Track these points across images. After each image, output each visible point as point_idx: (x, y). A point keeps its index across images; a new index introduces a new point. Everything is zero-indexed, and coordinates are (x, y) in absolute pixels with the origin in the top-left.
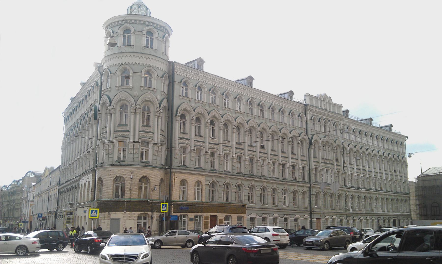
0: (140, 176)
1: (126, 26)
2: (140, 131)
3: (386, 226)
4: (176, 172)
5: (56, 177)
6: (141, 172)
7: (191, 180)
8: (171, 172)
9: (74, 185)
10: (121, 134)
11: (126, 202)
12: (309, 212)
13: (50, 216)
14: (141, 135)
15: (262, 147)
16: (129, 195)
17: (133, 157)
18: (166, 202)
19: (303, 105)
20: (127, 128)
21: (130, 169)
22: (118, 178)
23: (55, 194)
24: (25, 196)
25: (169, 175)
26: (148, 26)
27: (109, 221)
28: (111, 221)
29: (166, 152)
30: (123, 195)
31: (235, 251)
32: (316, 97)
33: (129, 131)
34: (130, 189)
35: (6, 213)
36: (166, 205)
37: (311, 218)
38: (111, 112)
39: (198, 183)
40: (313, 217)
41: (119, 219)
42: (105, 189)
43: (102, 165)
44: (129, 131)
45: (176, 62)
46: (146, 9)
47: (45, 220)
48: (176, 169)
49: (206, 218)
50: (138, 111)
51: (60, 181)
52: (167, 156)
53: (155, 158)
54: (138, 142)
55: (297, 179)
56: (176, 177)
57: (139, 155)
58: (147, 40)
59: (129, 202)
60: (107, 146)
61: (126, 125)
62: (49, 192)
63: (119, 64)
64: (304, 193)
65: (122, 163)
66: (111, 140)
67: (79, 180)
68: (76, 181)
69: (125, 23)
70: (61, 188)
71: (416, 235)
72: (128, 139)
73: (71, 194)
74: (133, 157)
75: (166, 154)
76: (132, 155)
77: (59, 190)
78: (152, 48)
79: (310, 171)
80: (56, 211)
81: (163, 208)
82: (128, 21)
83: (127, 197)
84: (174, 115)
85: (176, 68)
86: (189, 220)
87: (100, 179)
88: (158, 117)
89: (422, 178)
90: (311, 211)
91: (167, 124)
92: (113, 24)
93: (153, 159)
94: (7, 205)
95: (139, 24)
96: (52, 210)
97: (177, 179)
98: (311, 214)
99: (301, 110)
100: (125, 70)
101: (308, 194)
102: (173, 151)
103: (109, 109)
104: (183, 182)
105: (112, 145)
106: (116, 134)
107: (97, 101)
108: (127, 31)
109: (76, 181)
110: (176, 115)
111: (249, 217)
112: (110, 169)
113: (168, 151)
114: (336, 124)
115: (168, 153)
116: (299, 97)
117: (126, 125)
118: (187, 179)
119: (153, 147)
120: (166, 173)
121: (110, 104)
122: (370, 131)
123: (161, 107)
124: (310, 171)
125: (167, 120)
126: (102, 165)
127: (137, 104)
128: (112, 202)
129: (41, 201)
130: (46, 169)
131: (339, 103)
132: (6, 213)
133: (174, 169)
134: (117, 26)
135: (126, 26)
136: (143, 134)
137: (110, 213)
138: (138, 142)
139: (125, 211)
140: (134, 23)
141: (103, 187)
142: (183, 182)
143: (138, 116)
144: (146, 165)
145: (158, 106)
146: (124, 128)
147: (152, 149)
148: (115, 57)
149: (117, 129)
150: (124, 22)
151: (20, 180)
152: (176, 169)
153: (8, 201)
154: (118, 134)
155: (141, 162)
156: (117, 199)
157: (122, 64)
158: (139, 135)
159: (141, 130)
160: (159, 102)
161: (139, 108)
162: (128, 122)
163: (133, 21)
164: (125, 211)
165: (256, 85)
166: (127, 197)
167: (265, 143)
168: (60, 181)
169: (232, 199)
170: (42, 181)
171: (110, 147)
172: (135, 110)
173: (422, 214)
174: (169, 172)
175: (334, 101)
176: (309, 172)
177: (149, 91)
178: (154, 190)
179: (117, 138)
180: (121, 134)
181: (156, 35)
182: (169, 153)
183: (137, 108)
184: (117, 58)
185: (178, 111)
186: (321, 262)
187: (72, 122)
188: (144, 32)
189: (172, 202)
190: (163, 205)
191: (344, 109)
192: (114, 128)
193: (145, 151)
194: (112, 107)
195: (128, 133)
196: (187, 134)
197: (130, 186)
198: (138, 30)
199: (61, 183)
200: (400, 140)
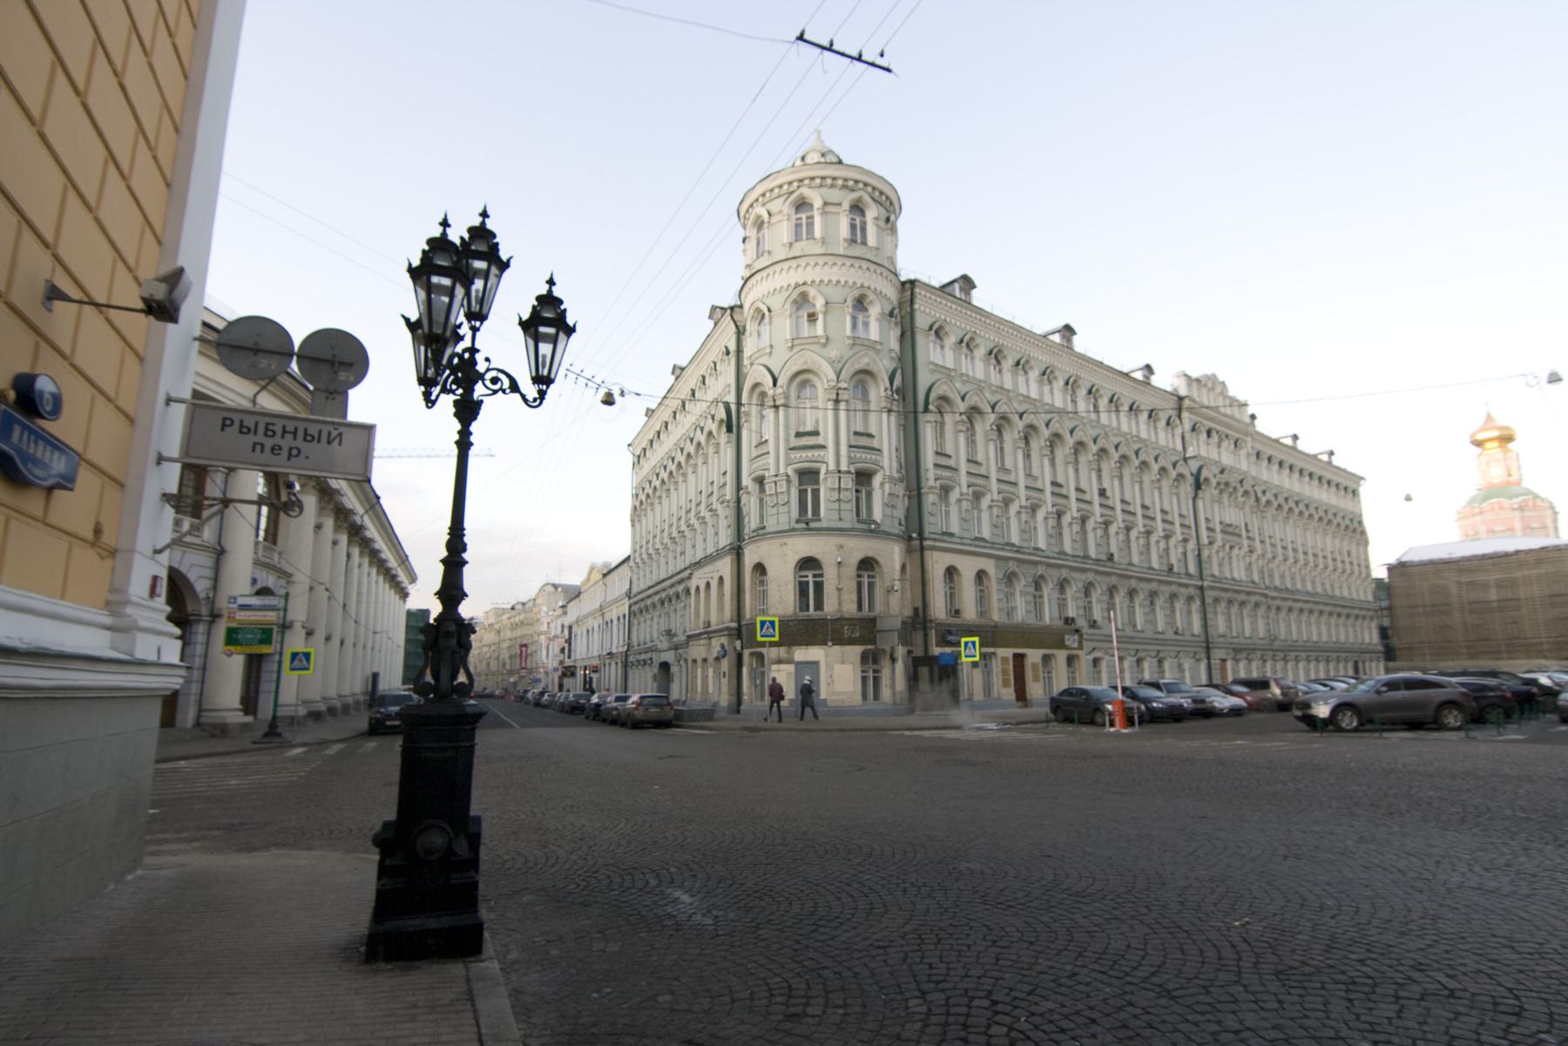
0: (858, 556)
1: (801, 194)
2: (851, 446)
3: (1342, 673)
4: (933, 548)
5: (619, 584)
6: (860, 548)
7: (967, 567)
8: (922, 549)
9: (642, 604)
11: (831, 620)
12: (1204, 644)
13: (610, 664)
14: (852, 455)
15: (1102, 493)
16: (836, 603)
17: (840, 510)
19: (1176, 398)
20: (820, 440)
21: (834, 541)
22: (808, 563)
23: (619, 618)
24: (545, 628)
25: (917, 555)
26: (853, 190)
29: (906, 499)
30: (819, 605)
31: (432, 696)
32: (1198, 380)
33: (823, 447)
34: (839, 589)
35: (508, 662)
36: (974, 643)
37: (1209, 658)
38: (779, 402)
39: (981, 576)
40: (1212, 656)
41: (816, 663)
42: (772, 589)
43: (761, 533)
44: (823, 447)
45: (919, 281)
47: (596, 671)
48: (935, 540)
49: (1005, 660)
50: (843, 396)
51: (630, 589)
52: (908, 510)
53: (888, 511)
54: (849, 472)
55: (1175, 570)
56: (934, 559)
58: (853, 227)
59: (840, 620)
60: (773, 485)
62: (603, 615)
63: (789, 286)
64: (1190, 599)
65: (812, 525)
66: (782, 471)
67: (689, 578)
68: (681, 581)
69: (799, 187)
70: (636, 603)
72: (825, 465)
73: (642, 620)
74: (840, 510)
75: (906, 504)
76: (836, 506)
77: (630, 607)
78: (864, 243)
80: (628, 650)
82: (807, 182)
83: (830, 606)
84: (921, 407)
85: (918, 296)
87: (760, 569)
89: (1398, 569)
90: (1207, 641)
91: (902, 433)
92: (768, 195)
93: (884, 515)
94: (509, 648)
95: (832, 186)
96: (614, 651)
97: (937, 563)
98: (1208, 648)
99: (1169, 406)
101: (1198, 603)
102: (924, 498)
103: (773, 397)
104: (951, 572)
105: (784, 483)
106: (793, 456)
107: (729, 392)
108: (802, 205)
109: (681, 581)
110: (926, 410)
111: (1091, 657)
112: (785, 540)
113: (909, 497)
115: (909, 503)
116: (1162, 380)
117: (816, 433)
118: (959, 567)
120: (909, 551)
121: (775, 384)
123: (894, 388)
124: (1199, 550)
125: (902, 422)
126: (761, 532)
127: (841, 377)
129: (585, 633)
130: (592, 569)
131: (1241, 398)
132: (508, 662)
133: (929, 539)
134: (779, 196)
135: (801, 194)
136: (859, 455)
137: (794, 648)
138: (849, 472)
139: (830, 644)
140: (821, 186)
141: (770, 587)
142: (951, 572)
144: (872, 530)
145: (888, 385)
148: (778, 270)
149: (795, 442)
150: (795, 184)
151: (529, 600)
152: (935, 540)
153: (510, 640)
156: (807, 613)
157: (797, 286)
159: (853, 443)
161: (845, 389)
164: (830, 644)
165: (1080, 344)
166: (830, 606)
167: (1106, 485)
168: (630, 589)
169: (1049, 616)
170: (582, 596)
171: (781, 487)
172: (838, 394)
174: (918, 548)
175: (1231, 393)
178: (890, 590)
182: (915, 500)
183: (840, 388)
184: (784, 273)
185: (931, 400)
187: (647, 466)
188: (846, 206)
189: (931, 621)
191: (1250, 410)
192: (787, 440)
194: (779, 391)
195: (822, 453)
196: (949, 457)
197: (837, 581)
198: (829, 200)
199: (635, 590)
200: (1352, 486)
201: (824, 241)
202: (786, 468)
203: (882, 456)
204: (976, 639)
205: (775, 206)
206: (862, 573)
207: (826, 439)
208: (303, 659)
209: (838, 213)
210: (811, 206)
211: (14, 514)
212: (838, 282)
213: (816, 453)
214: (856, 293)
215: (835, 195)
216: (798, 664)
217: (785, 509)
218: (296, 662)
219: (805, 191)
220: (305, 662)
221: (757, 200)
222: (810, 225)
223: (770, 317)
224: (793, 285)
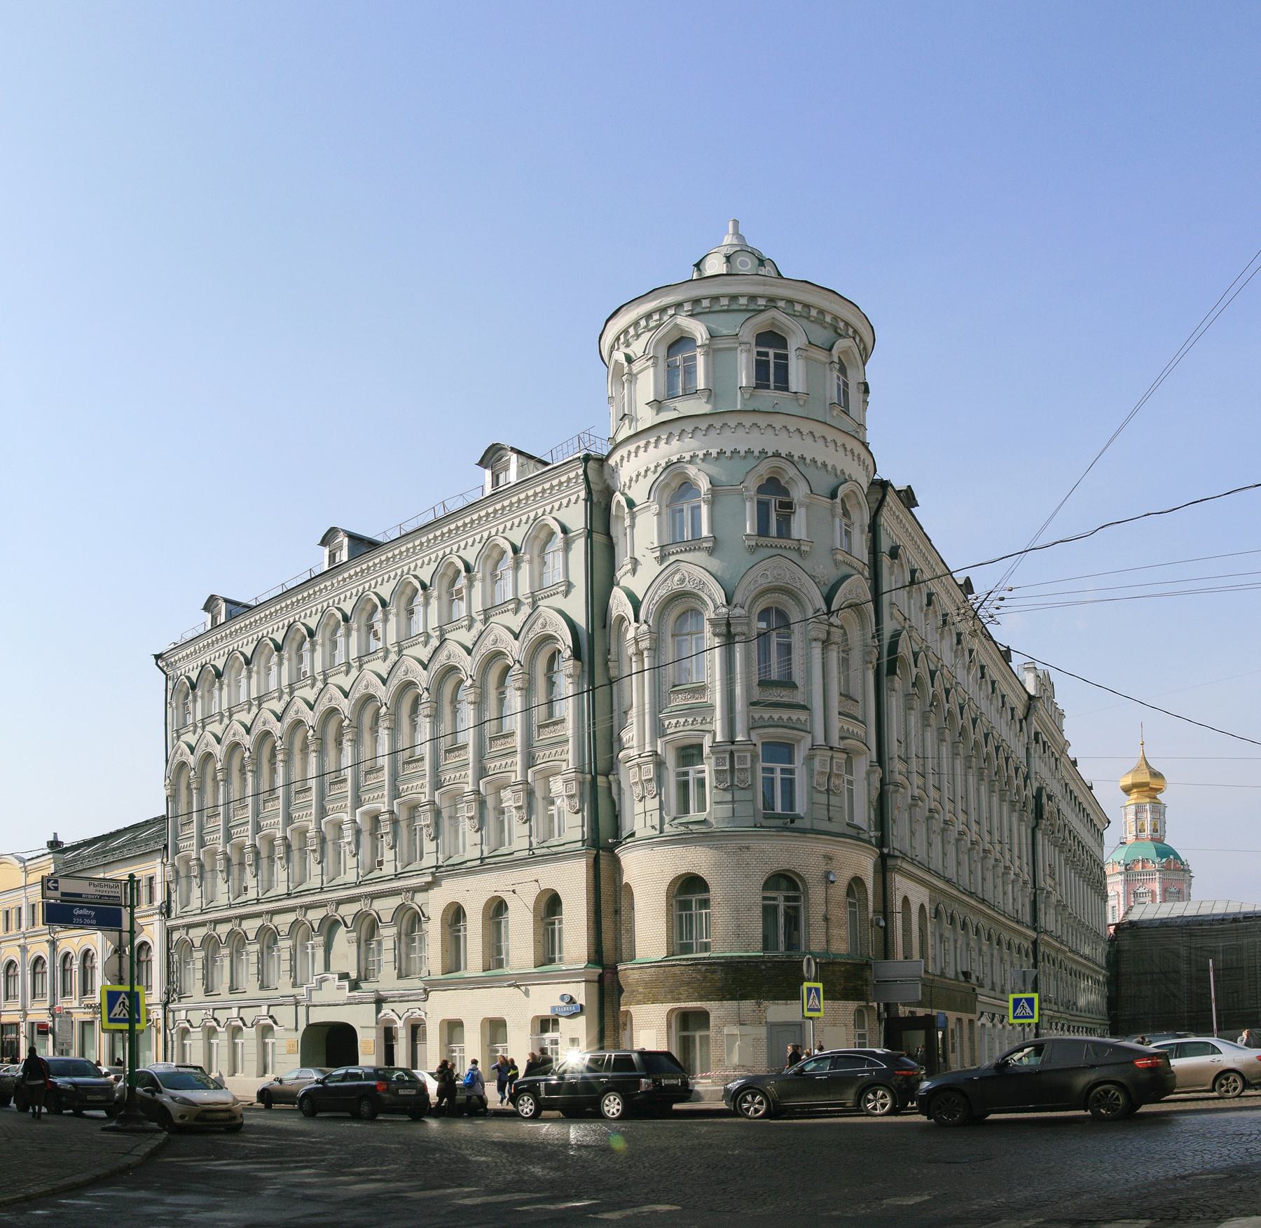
2: (753, 704)
10: (776, 716)
14: (757, 716)
18: (815, 981)
21: (820, 847)
27: (762, 1031)
28: (770, 1033)
36: (817, 990)
46: (757, 262)
57: (754, 795)
61: (788, 684)
71: (683, 1206)
76: (822, 798)
79: (1035, 894)
81: (810, 1003)
86: (126, 913)
88: (826, 643)
100: (773, 485)
114: (687, 640)
119: (810, 759)
122: (993, 673)
124: (1035, 894)
128: (769, 965)
143: (739, 650)
146: (784, 696)
147: (804, 767)
149: (757, 694)
154: (766, 714)
155: (766, 817)
158: (750, 718)
160: (826, 590)
162: (798, 677)
163: (798, 307)
173: (540, 1064)
176: (1032, 899)
177: (780, 551)
179: (771, 730)
180: (776, 716)
181: (795, 342)
186: (468, 1202)
190: (809, 990)
193: (778, 776)
201: (710, 393)
202: (653, 743)
203: (811, 715)
204: (820, 985)
205: (637, 348)
206: (688, 897)
207: (809, 694)
208: (1026, 1005)
209: (736, 349)
210: (693, 340)
211: (913, 820)
212: (721, 453)
213: (796, 715)
214: (764, 469)
215: (727, 324)
216: (772, 1026)
217: (747, 795)
218: (1018, 1010)
219: (684, 321)
220: (1028, 1010)
221: (618, 339)
222: (690, 371)
223: (633, 517)
224: (664, 465)
